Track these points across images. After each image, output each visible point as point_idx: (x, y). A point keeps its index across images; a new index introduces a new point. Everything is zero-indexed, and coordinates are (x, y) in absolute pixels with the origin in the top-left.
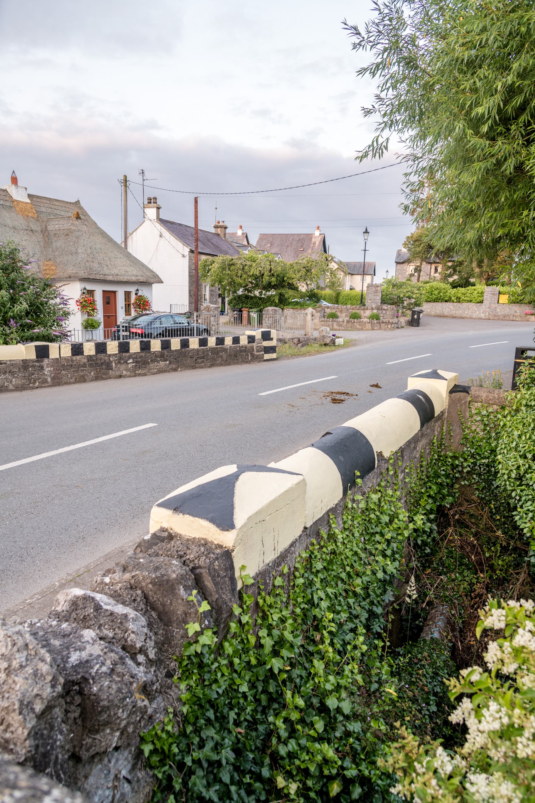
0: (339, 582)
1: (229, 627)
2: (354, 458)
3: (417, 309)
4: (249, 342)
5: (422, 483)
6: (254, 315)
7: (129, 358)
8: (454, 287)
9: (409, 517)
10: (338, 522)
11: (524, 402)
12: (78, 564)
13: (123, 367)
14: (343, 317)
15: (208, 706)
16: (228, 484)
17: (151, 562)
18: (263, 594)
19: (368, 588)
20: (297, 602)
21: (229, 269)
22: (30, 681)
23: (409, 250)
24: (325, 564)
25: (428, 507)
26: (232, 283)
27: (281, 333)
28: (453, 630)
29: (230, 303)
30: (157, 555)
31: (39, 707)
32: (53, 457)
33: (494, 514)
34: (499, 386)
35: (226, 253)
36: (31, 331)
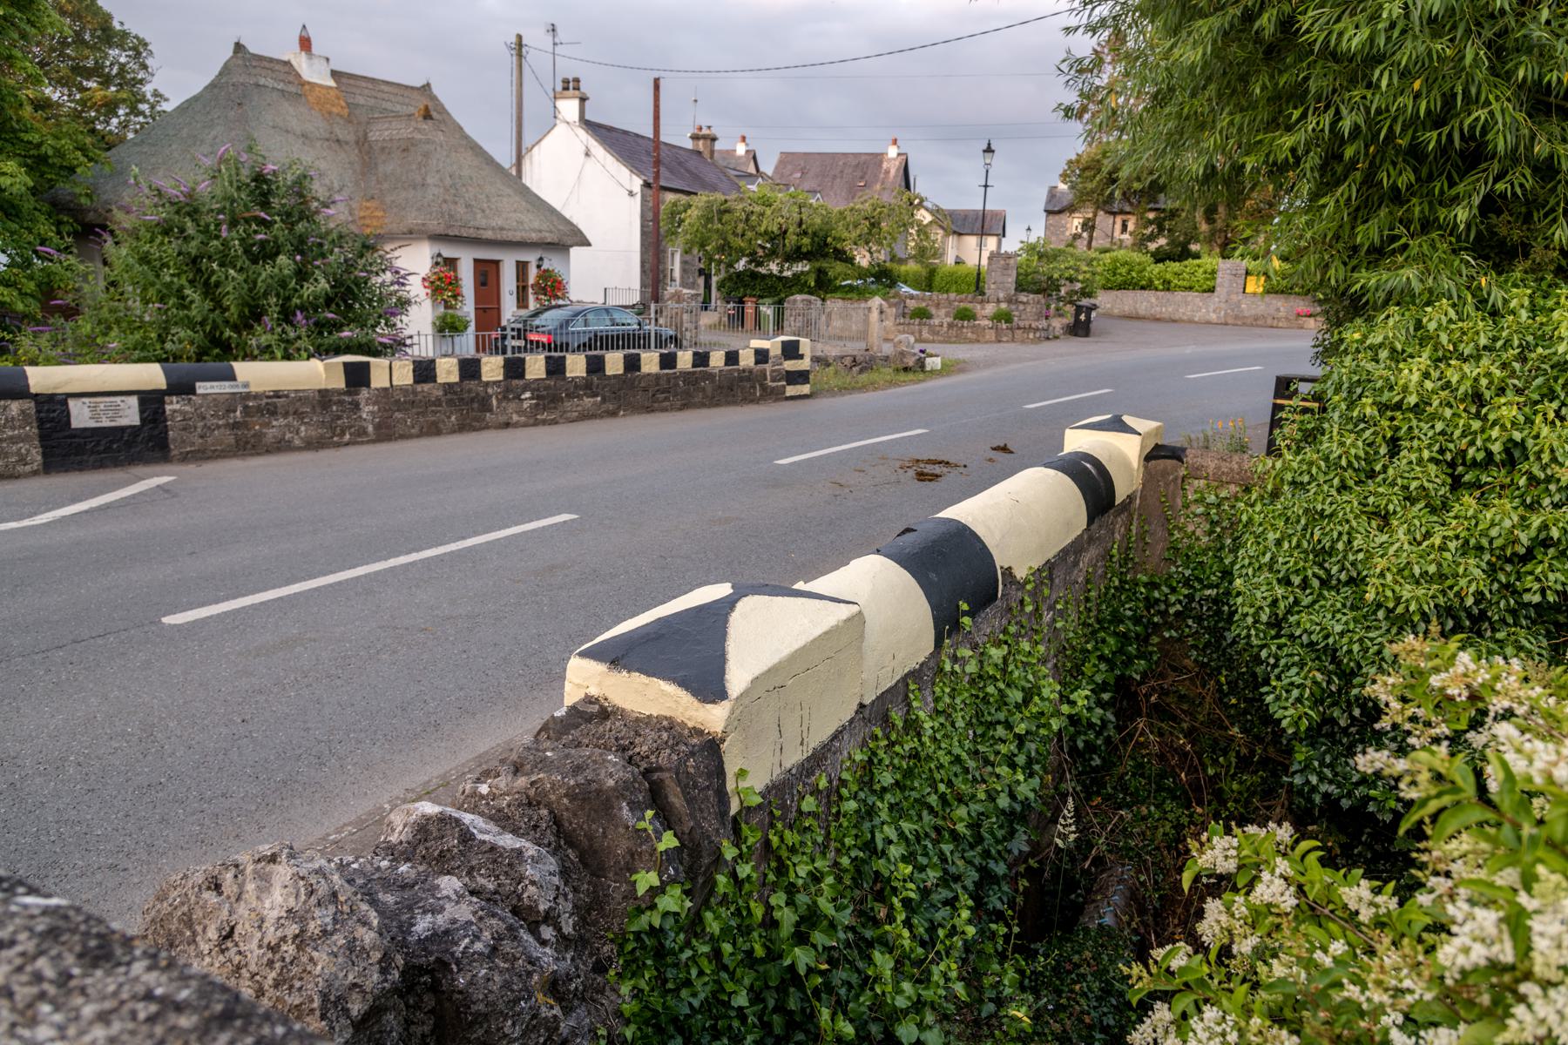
0: (925, 813)
1: (715, 883)
2: (957, 577)
3: (1085, 302)
4: (757, 363)
5: (1088, 631)
6: (767, 310)
7: (524, 390)
8: (1158, 261)
9: (1060, 693)
10: (924, 699)
11: (1289, 476)
12: (430, 773)
13: (512, 407)
14: (941, 317)
15: (671, 1029)
16: (715, 618)
17: (567, 756)
18: (779, 825)
19: (979, 826)
20: (843, 844)
21: (720, 220)
22: (340, 960)
23: (1072, 188)
24: (898, 776)
25: (1099, 679)
26: (725, 247)
27: (819, 346)
28: (1142, 911)
29: (721, 286)
30: (579, 745)
31: (356, 1007)
32: (377, 573)
33: (1226, 695)
34: (1242, 448)
35: (714, 189)
36: (336, 335)
